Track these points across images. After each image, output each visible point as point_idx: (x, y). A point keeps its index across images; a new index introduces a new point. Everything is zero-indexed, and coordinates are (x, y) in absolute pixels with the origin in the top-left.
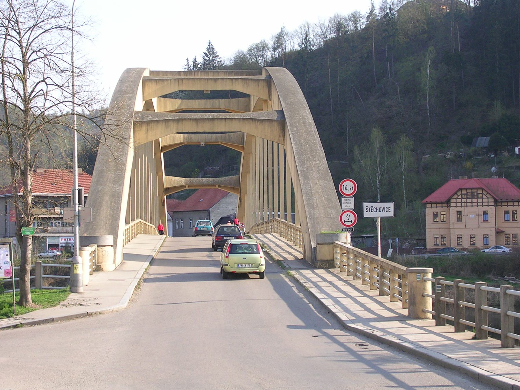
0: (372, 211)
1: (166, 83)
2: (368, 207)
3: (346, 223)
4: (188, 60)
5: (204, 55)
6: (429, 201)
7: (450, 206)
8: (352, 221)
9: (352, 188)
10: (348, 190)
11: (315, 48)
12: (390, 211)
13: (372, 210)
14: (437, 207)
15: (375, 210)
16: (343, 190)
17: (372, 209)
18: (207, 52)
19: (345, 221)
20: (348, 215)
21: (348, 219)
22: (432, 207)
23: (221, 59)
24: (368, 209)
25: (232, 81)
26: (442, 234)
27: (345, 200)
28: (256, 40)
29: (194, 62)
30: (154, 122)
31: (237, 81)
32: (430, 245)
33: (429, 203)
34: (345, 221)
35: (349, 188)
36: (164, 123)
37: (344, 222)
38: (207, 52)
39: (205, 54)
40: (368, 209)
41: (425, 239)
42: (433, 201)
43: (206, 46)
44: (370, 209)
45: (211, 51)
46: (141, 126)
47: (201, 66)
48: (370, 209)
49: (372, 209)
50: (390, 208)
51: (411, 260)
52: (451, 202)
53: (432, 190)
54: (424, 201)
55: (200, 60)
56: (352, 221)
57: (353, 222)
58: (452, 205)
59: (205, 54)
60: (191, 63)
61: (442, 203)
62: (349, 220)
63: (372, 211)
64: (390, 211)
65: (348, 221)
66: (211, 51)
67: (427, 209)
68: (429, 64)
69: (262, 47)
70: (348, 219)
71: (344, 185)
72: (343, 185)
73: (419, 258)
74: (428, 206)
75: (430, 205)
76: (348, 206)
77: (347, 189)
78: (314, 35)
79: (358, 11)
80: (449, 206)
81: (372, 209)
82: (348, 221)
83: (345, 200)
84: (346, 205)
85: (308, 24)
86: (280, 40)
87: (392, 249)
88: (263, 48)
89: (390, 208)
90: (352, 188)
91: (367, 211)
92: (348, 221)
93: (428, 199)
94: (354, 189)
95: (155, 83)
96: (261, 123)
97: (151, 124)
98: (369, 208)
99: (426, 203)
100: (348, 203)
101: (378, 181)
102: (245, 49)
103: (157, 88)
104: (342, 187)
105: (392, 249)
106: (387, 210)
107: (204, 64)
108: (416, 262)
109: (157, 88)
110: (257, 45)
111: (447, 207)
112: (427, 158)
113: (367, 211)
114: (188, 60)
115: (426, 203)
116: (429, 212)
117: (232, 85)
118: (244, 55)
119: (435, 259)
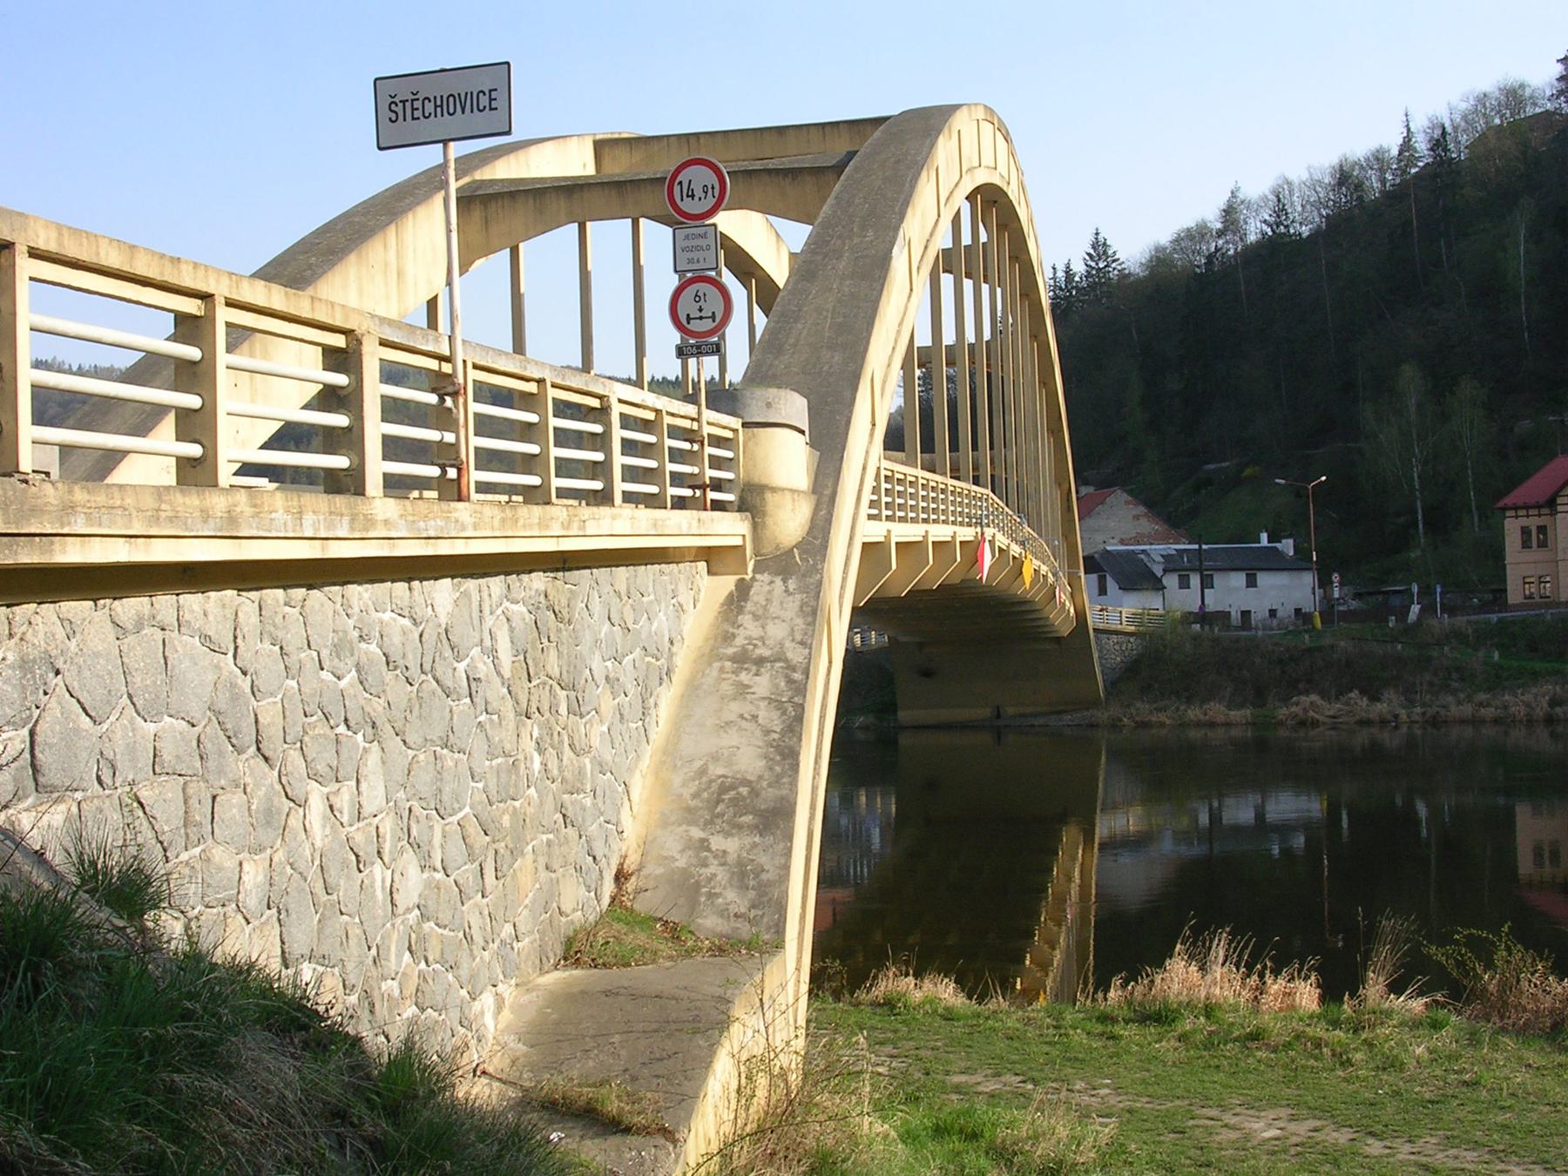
0: (416, 114)
1: (656, 148)
2: (396, 100)
3: (695, 326)
4: (1054, 268)
5: (1087, 258)
6: (1510, 504)
7: (1556, 514)
8: (713, 317)
9: (710, 190)
10: (696, 198)
11: (1305, 231)
12: (494, 104)
13: (413, 109)
14: (1528, 516)
15: (429, 107)
16: (678, 198)
17: (416, 104)
18: (1092, 252)
19: (689, 319)
20: (701, 294)
21: (701, 310)
22: (1517, 517)
23: (1123, 266)
24: (399, 109)
25: (823, 128)
26: (1541, 574)
27: (687, 237)
28: (1190, 221)
29: (1067, 272)
30: (503, 198)
31: (836, 131)
32: (1514, 596)
33: (1511, 509)
34: (689, 319)
35: (699, 193)
36: (531, 201)
37: (684, 321)
38: (1092, 252)
39: (1089, 254)
40: (399, 109)
41: (1506, 590)
42: (1520, 503)
43: (1090, 238)
44: (408, 105)
45: (1100, 249)
46: (469, 210)
47: (1081, 278)
48: (408, 105)
49: (416, 104)
50: (494, 95)
51: (1460, 628)
52: (1559, 502)
53: (1513, 483)
54: (1501, 504)
55: (1079, 268)
56: (713, 317)
57: (718, 320)
58: (1559, 508)
59: (1089, 254)
60: (1061, 274)
61: (1539, 507)
62: (703, 314)
63: (416, 114)
64: (494, 104)
65: (701, 318)
66: (1100, 249)
67: (1507, 521)
68: (1523, 232)
69: (1198, 234)
70: (701, 310)
71: (680, 183)
72: (677, 181)
73: (1476, 623)
74: (1508, 513)
75: (1512, 513)
76: (698, 261)
77: (693, 196)
78: (1302, 205)
79: (1385, 146)
80: (1554, 513)
81: (418, 104)
82: (699, 315)
83: (687, 237)
84: (690, 255)
85: (1288, 183)
86: (1230, 214)
87: (1419, 606)
88: (1203, 236)
89: (494, 95)
90: (710, 190)
91: (393, 117)
92: (701, 318)
93: (1508, 500)
94: (716, 195)
95: (628, 149)
96: (793, 179)
97: (493, 204)
98: (404, 102)
99: (1504, 509)
100: (699, 248)
101: (1415, 475)
102: (1164, 237)
103: (633, 161)
104: (677, 189)
105: (1419, 606)
106: (484, 101)
107: (1088, 275)
108: (1470, 631)
109: (633, 161)
110: (1188, 230)
111: (1551, 515)
112: (1525, 426)
113: (393, 117)
114: (1054, 268)
115: (1504, 509)
116: (1512, 528)
117: (824, 137)
118: (1165, 249)
119: (1513, 622)
